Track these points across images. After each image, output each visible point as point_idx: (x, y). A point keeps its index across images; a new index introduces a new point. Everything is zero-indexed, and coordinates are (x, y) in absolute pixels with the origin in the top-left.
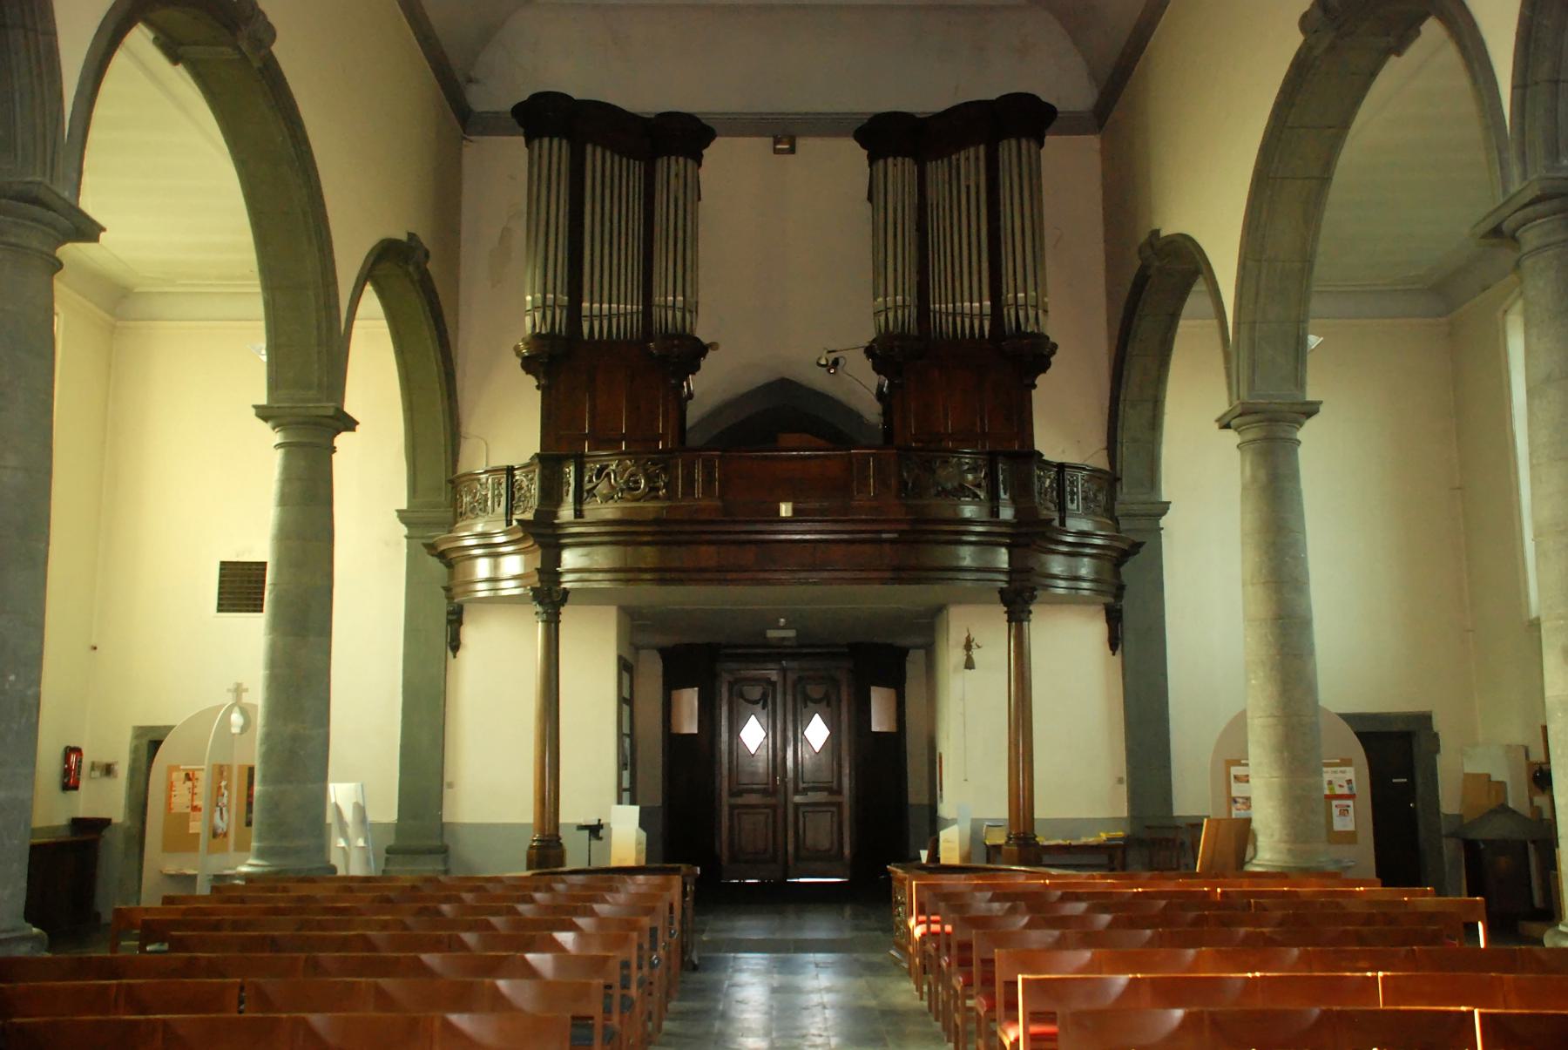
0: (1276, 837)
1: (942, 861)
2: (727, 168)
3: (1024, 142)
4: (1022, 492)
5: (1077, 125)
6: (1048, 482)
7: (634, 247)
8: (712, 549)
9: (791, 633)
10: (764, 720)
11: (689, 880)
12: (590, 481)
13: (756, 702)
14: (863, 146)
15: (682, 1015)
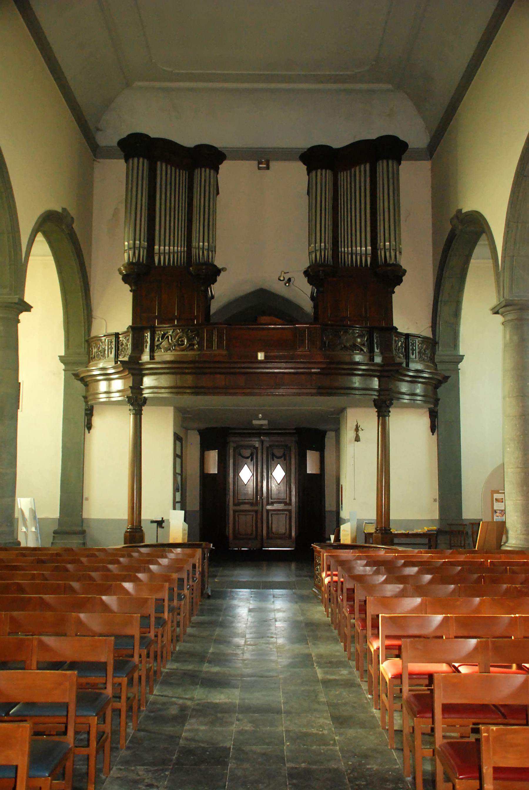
0: (519, 532)
1: (342, 542)
2: (231, 175)
3: (390, 162)
4: (386, 348)
5: (418, 155)
6: (400, 344)
7: (182, 216)
8: (223, 377)
9: (265, 422)
10: (251, 467)
11: (206, 551)
12: (158, 340)
13: (248, 458)
14: (305, 164)
15: (200, 624)
